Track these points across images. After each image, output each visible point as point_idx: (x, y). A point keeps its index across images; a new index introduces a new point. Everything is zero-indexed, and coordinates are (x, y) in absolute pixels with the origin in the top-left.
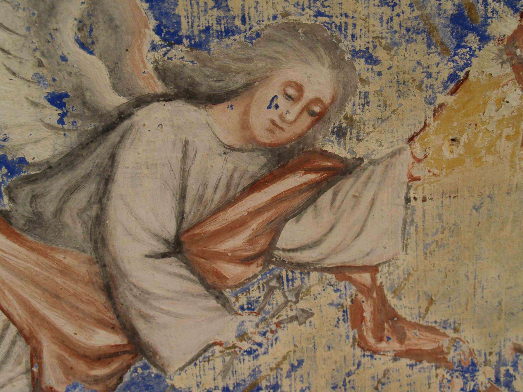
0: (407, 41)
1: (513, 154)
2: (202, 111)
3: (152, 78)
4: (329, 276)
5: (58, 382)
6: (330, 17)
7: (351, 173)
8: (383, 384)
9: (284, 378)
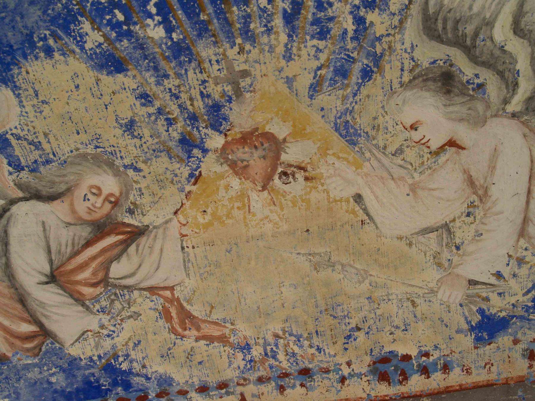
0: (156, 157)
1: (245, 218)
2: (47, 205)
3: (15, 189)
4: (145, 293)
5: (7, 351)
6: (104, 148)
7: (144, 234)
8: (192, 355)
9: (131, 350)
